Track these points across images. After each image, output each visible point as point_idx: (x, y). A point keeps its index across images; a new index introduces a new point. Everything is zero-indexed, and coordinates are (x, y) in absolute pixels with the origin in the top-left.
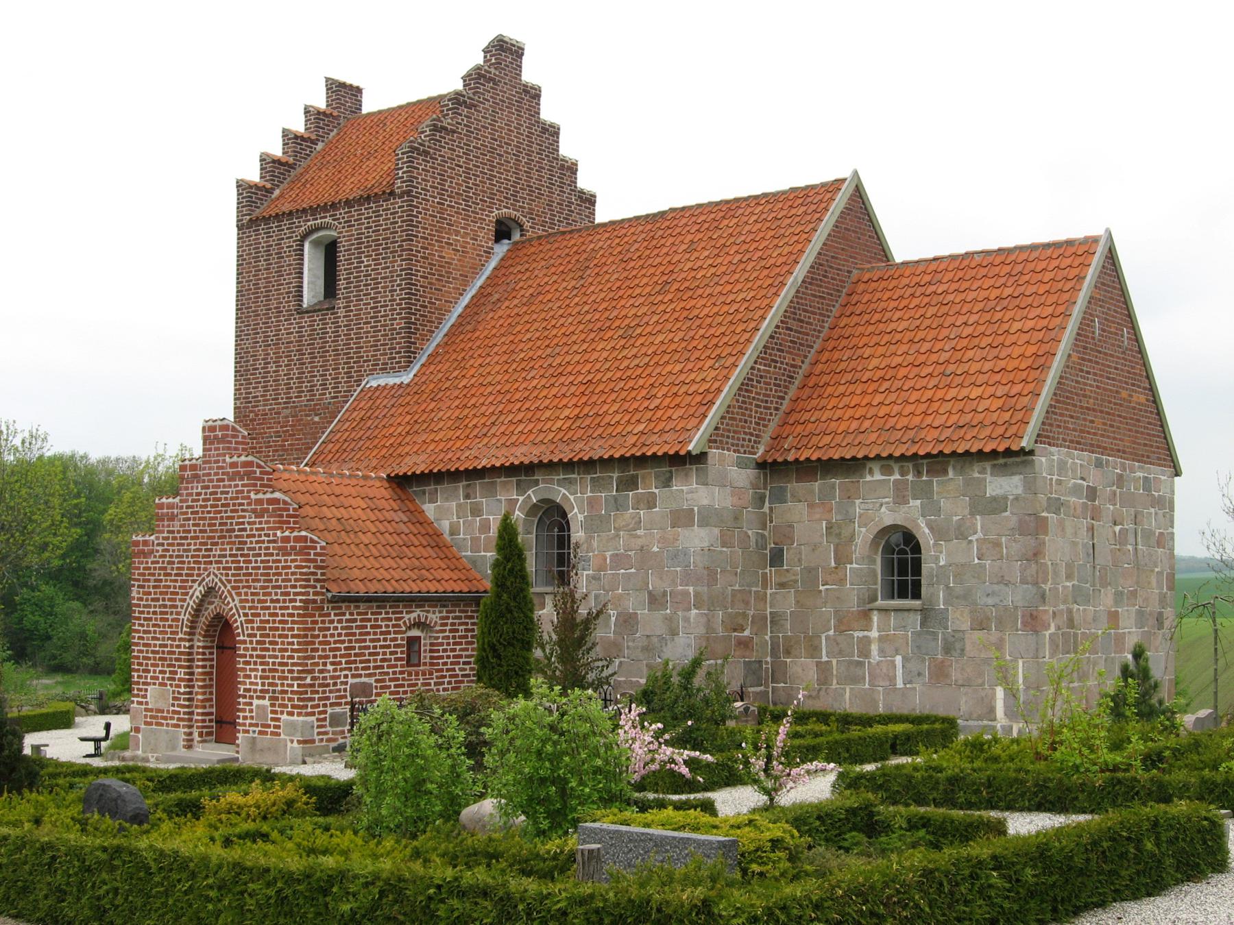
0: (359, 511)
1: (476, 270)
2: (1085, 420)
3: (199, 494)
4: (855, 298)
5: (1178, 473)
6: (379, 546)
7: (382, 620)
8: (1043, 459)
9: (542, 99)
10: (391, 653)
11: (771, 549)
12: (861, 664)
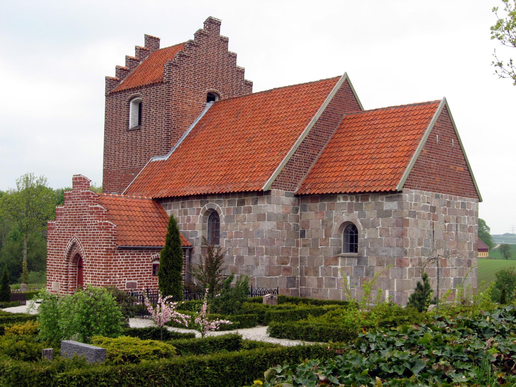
0: (137, 212)
1: (198, 114)
2: (430, 178)
3: (71, 205)
4: (343, 126)
5: (480, 201)
6: (144, 227)
7: (141, 257)
8: (407, 195)
9: (229, 43)
10: (145, 271)
11: (301, 231)
12: (334, 279)
